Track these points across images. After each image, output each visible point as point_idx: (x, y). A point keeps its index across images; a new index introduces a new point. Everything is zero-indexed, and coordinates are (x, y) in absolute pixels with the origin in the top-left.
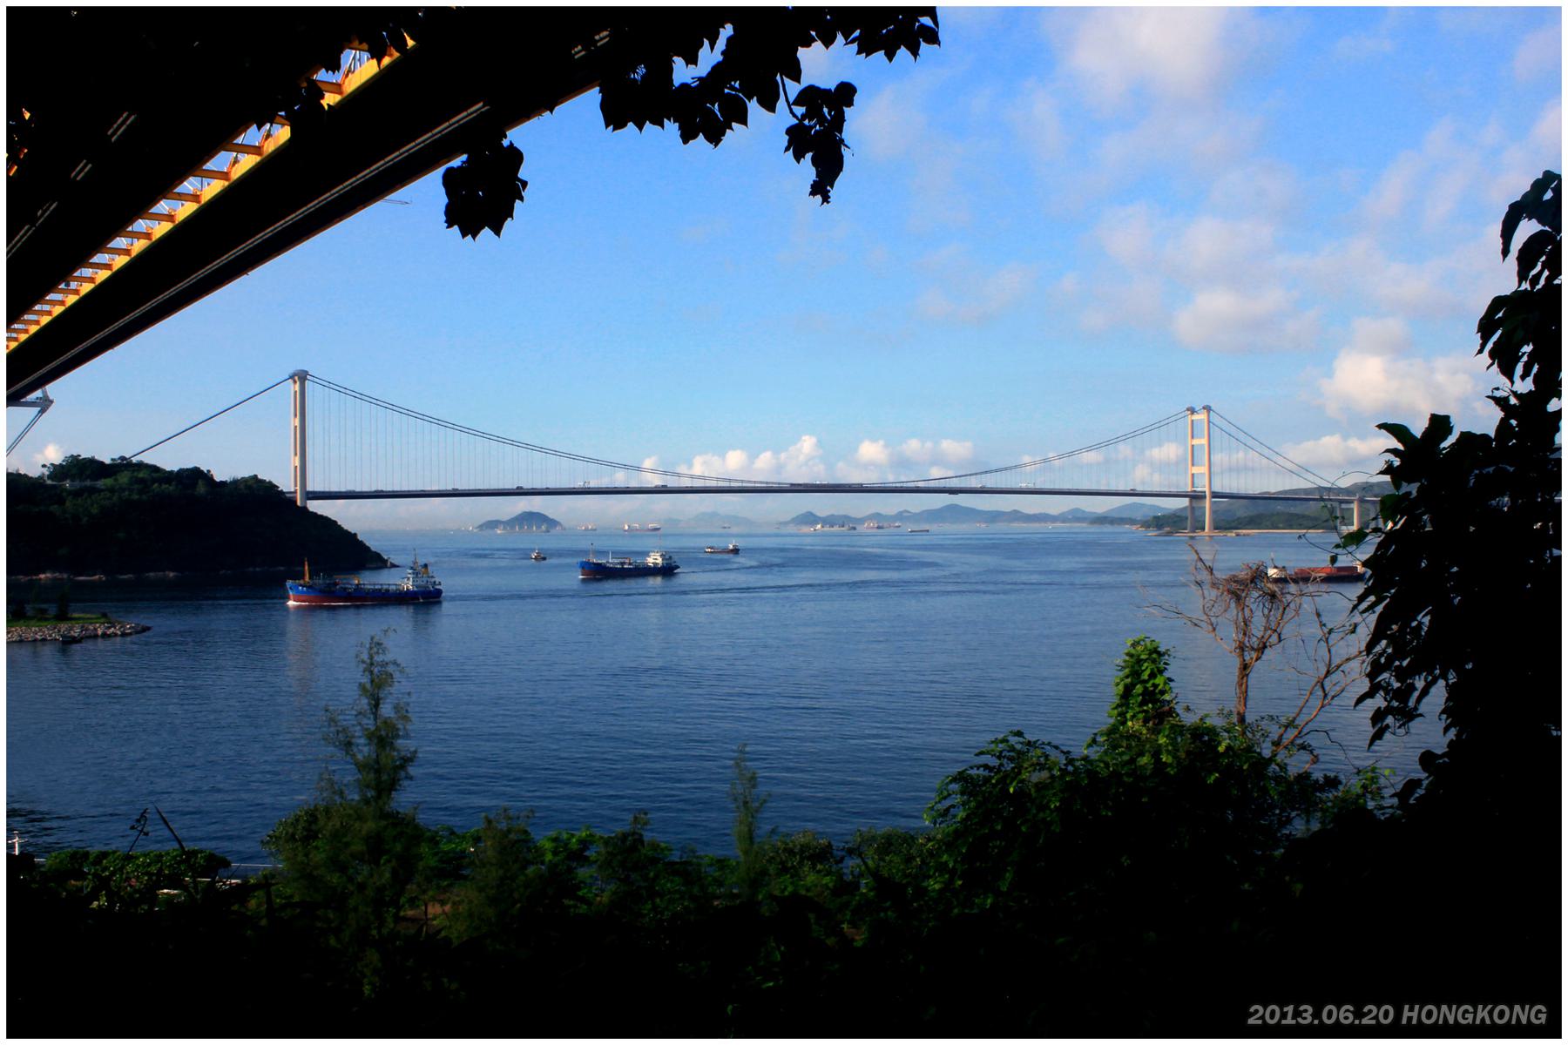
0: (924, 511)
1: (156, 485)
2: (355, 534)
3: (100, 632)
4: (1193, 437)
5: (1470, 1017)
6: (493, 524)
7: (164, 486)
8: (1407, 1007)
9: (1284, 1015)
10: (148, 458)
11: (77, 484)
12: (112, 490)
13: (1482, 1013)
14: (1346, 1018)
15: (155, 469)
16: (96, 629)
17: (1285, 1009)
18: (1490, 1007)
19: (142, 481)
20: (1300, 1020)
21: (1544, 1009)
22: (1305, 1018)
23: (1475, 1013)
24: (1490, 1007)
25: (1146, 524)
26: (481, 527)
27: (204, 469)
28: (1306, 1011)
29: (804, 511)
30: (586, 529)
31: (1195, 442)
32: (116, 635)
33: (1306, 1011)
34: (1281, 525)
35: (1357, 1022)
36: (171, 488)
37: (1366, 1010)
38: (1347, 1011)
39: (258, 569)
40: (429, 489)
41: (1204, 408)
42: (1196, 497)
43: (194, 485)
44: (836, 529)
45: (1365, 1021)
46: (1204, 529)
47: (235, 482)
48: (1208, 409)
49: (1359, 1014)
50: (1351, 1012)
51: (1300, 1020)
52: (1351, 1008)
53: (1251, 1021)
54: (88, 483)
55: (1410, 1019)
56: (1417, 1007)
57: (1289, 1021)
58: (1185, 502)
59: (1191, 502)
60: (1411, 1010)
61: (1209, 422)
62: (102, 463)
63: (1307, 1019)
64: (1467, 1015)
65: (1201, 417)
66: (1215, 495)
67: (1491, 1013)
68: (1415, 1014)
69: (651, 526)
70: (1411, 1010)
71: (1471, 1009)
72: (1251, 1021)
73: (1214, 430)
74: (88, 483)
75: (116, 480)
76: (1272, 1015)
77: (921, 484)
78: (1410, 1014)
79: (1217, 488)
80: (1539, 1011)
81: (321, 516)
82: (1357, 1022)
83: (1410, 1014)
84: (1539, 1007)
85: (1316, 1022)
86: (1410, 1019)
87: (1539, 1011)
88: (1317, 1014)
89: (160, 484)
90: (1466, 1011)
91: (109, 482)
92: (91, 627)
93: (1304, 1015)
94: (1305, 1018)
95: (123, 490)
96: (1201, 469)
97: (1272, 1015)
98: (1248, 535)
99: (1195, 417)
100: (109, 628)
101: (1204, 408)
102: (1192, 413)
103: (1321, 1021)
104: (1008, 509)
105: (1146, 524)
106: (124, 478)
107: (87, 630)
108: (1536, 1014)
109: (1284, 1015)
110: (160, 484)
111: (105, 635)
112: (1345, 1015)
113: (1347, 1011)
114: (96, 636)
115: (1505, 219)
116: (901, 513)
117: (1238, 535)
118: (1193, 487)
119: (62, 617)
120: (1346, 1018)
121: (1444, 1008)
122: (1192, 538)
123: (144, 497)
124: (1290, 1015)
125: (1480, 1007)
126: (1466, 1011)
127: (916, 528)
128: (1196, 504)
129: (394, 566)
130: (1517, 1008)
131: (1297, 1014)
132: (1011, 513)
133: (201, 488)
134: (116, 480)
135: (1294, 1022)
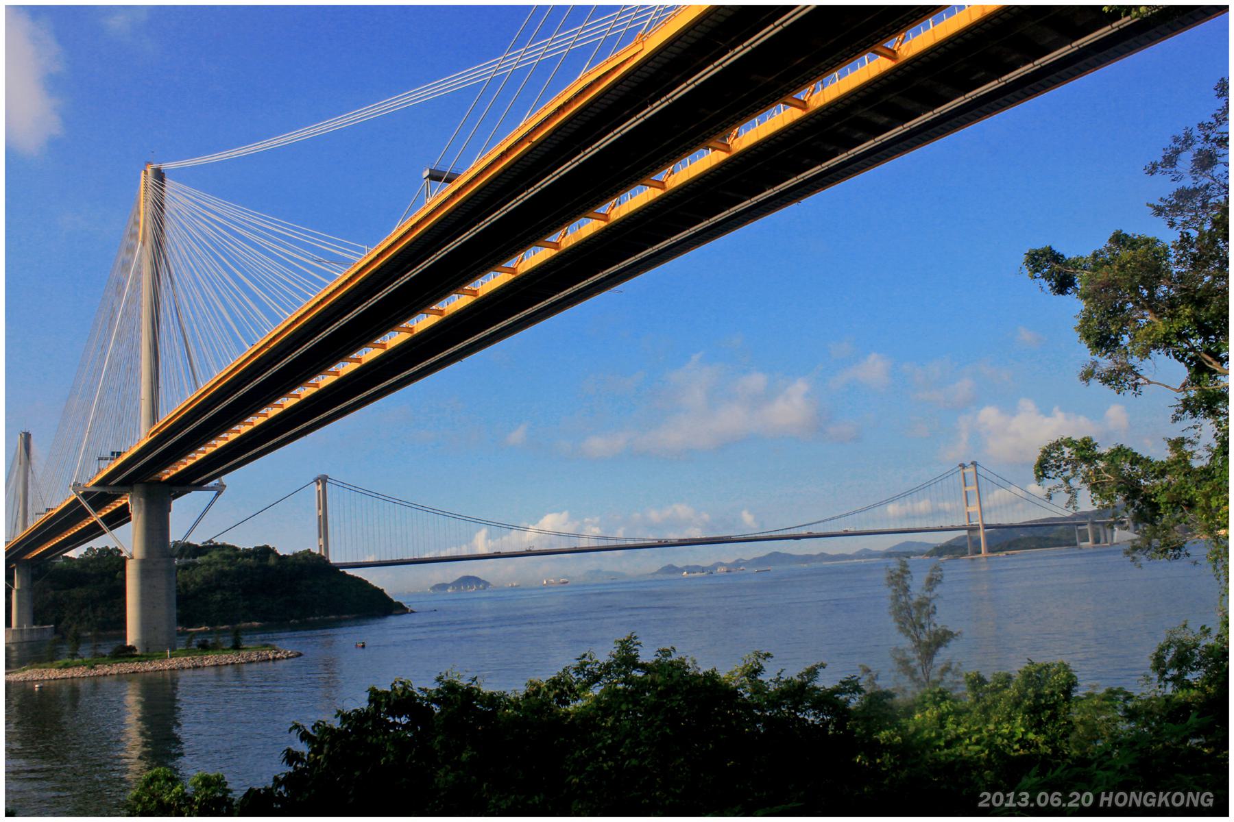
0: (755, 558)
1: (240, 559)
2: (382, 590)
3: (271, 657)
4: (965, 485)
5: (1153, 801)
6: (442, 587)
7: (246, 560)
8: (1103, 794)
9: (1006, 799)
10: (219, 541)
11: (183, 560)
12: (209, 564)
13: (1163, 798)
14: (1056, 802)
15: (235, 549)
16: (267, 655)
17: (1008, 795)
18: (1169, 793)
19: (228, 557)
20: (1019, 804)
21: (1211, 795)
22: (1024, 802)
23: (1157, 798)
24: (1169, 793)
25: (931, 554)
26: (433, 588)
27: (271, 547)
28: (1024, 796)
29: (666, 564)
30: (512, 586)
31: (968, 489)
32: (283, 658)
33: (1024, 796)
34: (1034, 546)
35: (1064, 805)
36: (251, 561)
37: (1071, 795)
38: (1057, 796)
39: (317, 618)
40: (406, 558)
41: (972, 463)
42: (973, 529)
43: (267, 558)
44: (698, 574)
45: (1071, 804)
46: (981, 553)
47: (295, 555)
48: (974, 464)
49: (1066, 799)
50: (1060, 797)
51: (1019, 804)
52: (1060, 794)
53: (981, 804)
54: (191, 560)
55: (1106, 803)
56: (1111, 794)
57: (1010, 804)
58: (965, 533)
59: (969, 533)
60: (1107, 795)
61: (977, 473)
62: (196, 545)
63: (1025, 803)
64: (1151, 800)
65: (970, 471)
66: (986, 527)
67: (1169, 798)
68: (1110, 799)
69: (562, 580)
70: (1107, 795)
71: (1154, 795)
72: (981, 804)
73: (982, 480)
74: (191, 560)
75: (210, 557)
76: (998, 800)
77: (774, 534)
78: (1106, 799)
79: (988, 521)
80: (1208, 797)
81: (357, 578)
82: (1064, 805)
83: (1106, 799)
84: (1150, 793)
85: (1032, 805)
86: (1106, 803)
87: (1208, 797)
88: (1032, 800)
89: (243, 558)
90: (1150, 797)
91: (205, 558)
92: (264, 653)
93: (1023, 799)
94: (1024, 802)
95: (216, 563)
96: (974, 508)
97: (998, 800)
98: (1015, 554)
99: (966, 471)
100: (277, 653)
101: (972, 463)
102: (963, 468)
103: (1036, 805)
104: (815, 553)
105: (931, 554)
106: (215, 555)
107: (261, 655)
108: (1206, 798)
109: (1006, 799)
110: (243, 558)
111: (275, 659)
112: (1055, 800)
113: (1057, 796)
114: (269, 659)
115: (363, 580)
116: (737, 561)
117: (1007, 554)
118: (969, 522)
119: (237, 647)
120: (1056, 802)
121: (1133, 794)
122: (973, 559)
123: (233, 568)
124: (1011, 799)
125: (1161, 793)
126: (1150, 797)
127: (760, 569)
128: (973, 534)
129: (412, 612)
130: (1190, 794)
131: (1017, 799)
132: (818, 555)
133: (272, 561)
134: (210, 557)
135: (1014, 805)
